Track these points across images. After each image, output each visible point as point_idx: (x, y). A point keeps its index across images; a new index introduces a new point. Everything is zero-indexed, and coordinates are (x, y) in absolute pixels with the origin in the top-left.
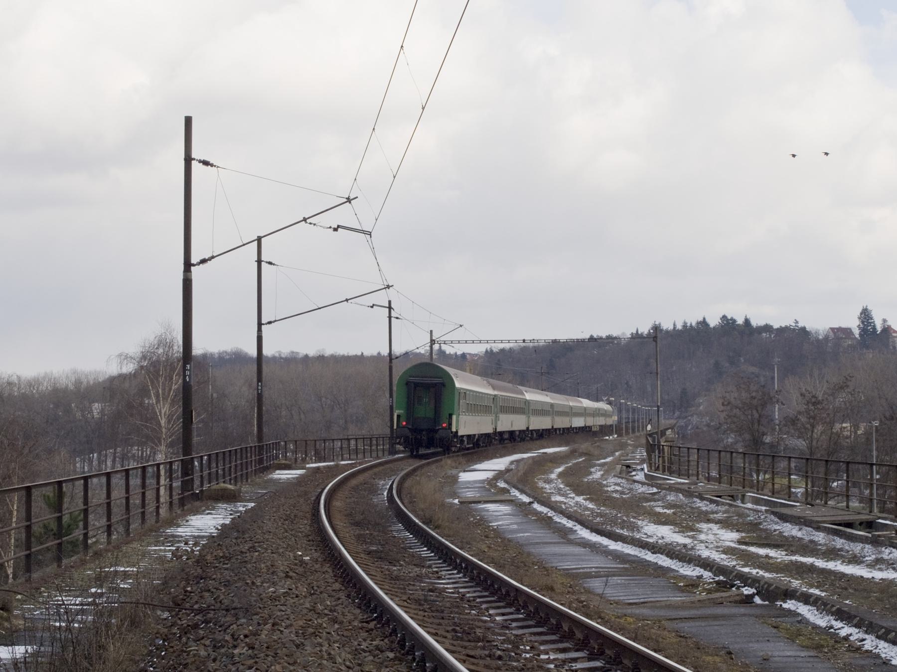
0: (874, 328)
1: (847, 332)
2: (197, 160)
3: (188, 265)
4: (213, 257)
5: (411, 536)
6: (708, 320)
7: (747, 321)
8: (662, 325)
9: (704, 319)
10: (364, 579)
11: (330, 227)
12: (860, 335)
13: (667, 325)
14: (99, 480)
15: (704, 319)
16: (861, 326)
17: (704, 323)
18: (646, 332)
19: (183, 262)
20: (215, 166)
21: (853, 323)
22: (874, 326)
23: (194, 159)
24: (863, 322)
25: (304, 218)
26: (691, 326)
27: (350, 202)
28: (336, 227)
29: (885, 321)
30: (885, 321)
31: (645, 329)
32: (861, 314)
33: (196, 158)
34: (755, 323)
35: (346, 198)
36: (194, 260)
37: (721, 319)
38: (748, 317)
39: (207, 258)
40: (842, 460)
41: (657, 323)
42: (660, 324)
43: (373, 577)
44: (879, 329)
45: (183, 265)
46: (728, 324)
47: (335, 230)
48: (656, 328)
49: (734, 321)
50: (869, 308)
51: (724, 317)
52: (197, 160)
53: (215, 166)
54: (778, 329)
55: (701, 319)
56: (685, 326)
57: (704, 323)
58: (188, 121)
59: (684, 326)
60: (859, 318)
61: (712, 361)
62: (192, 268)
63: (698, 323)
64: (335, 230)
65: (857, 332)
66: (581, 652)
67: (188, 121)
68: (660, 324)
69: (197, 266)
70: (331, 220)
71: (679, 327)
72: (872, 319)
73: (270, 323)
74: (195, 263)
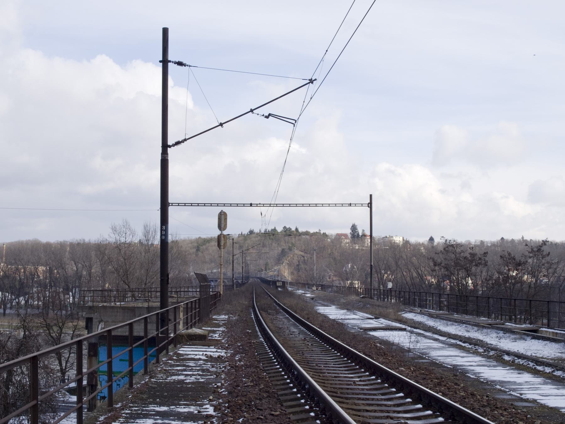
0: (358, 234)
1: (346, 236)
2: (173, 62)
3: (165, 146)
4: (185, 140)
5: (313, 336)
6: (277, 229)
7: (297, 229)
8: (254, 230)
9: (275, 228)
10: (400, 377)
11: (263, 115)
12: (351, 237)
13: (256, 230)
14: (159, 292)
15: (275, 228)
16: (352, 233)
17: (275, 230)
18: (246, 233)
19: (161, 145)
20: (188, 66)
21: (348, 231)
22: (358, 233)
23: (170, 61)
24: (353, 231)
25: (312, 83)
26: (269, 231)
27: (312, 83)
28: (267, 115)
29: (363, 231)
30: (363, 231)
31: (246, 232)
32: (352, 227)
33: (172, 60)
34: (300, 230)
35: (309, 80)
36: (170, 143)
37: (283, 228)
38: (297, 227)
39: (180, 140)
40: (495, 297)
41: (252, 229)
42: (253, 230)
43: (300, 363)
44: (360, 234)
45: (161, 148)
46: (287, 232)
47: (267, 117)
48: (251, 232)
49: (290, 229)
50: (356, 224)
51: (285, 227)
52: (173, 62)
53: (188, 66)
54: (312, 233)
55: (273, 228)
56: (266, 231)
57: (275, 230)
58: (165, 32)
59: (265, 231)
60: (351, 229)
61: (280, 249)
62: (169, 150)
63: (272, 230)
64: (267, 117)
65: (350, 236)
66: (412, 414)
67: (165, 32)
68: (253, 230)
69: (172, 147)
70: (266, 110)
71: (263, 231)
72: (357, 229)
73: (178, 143)
74: (171, 145)
